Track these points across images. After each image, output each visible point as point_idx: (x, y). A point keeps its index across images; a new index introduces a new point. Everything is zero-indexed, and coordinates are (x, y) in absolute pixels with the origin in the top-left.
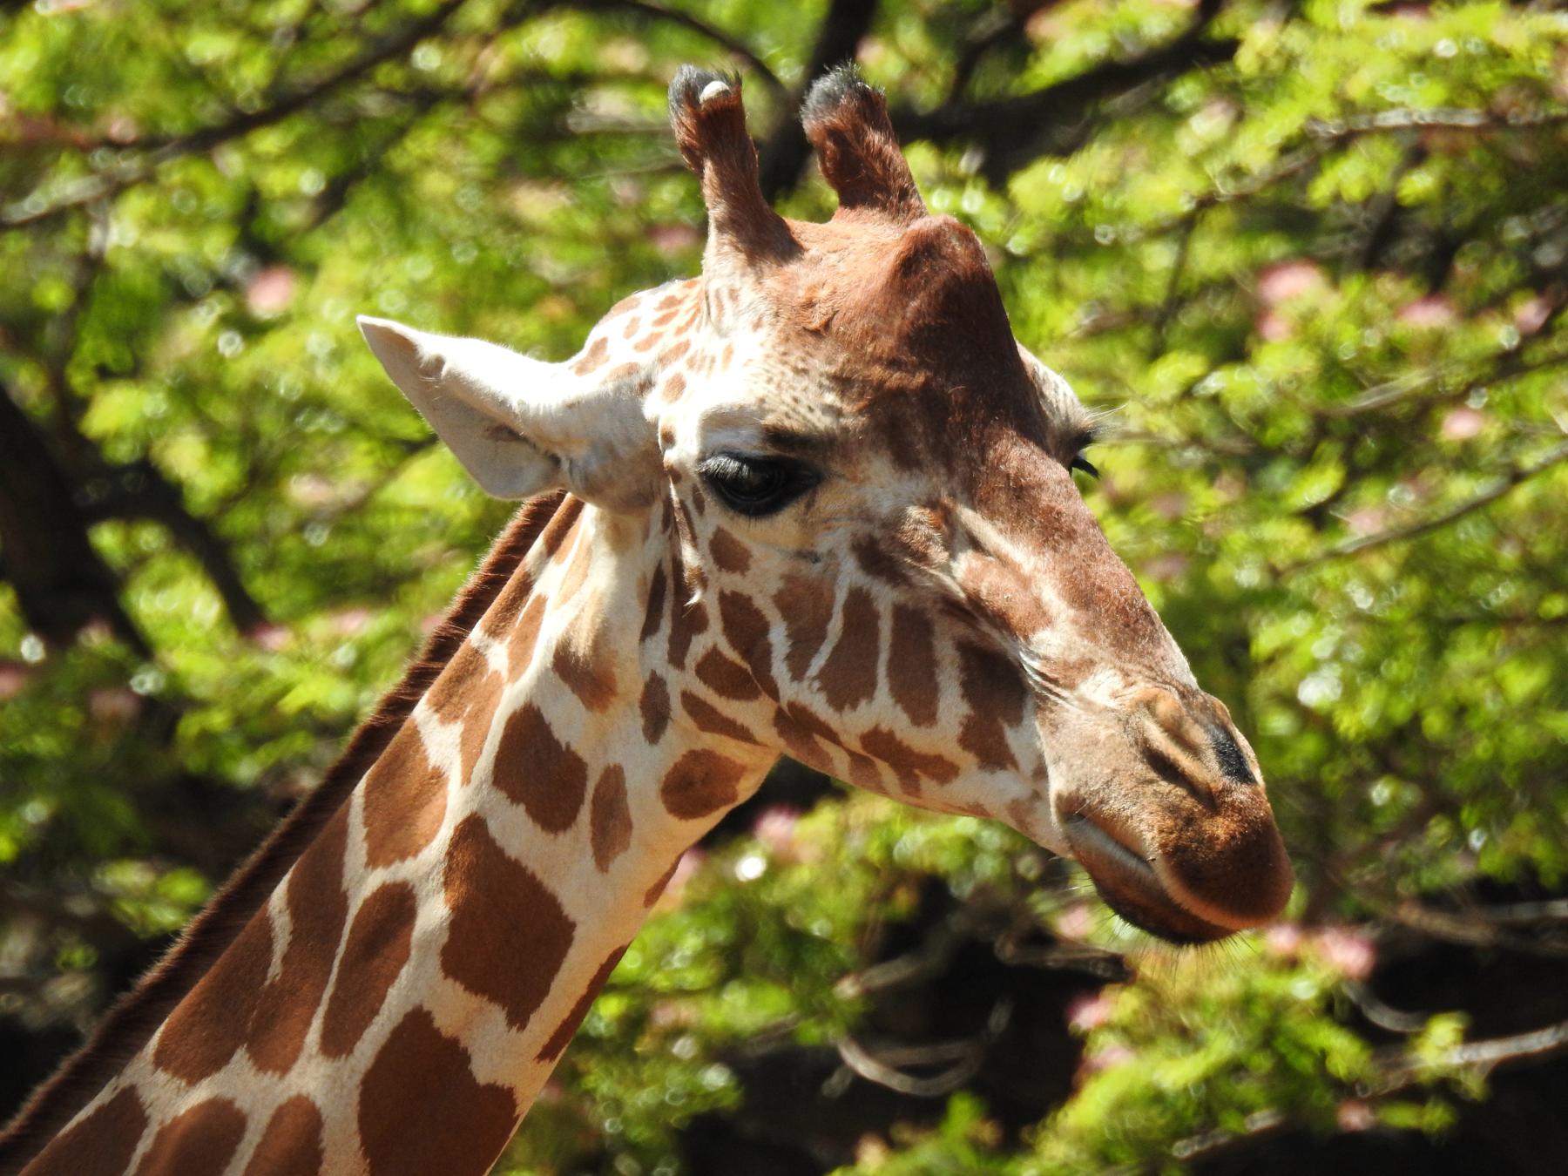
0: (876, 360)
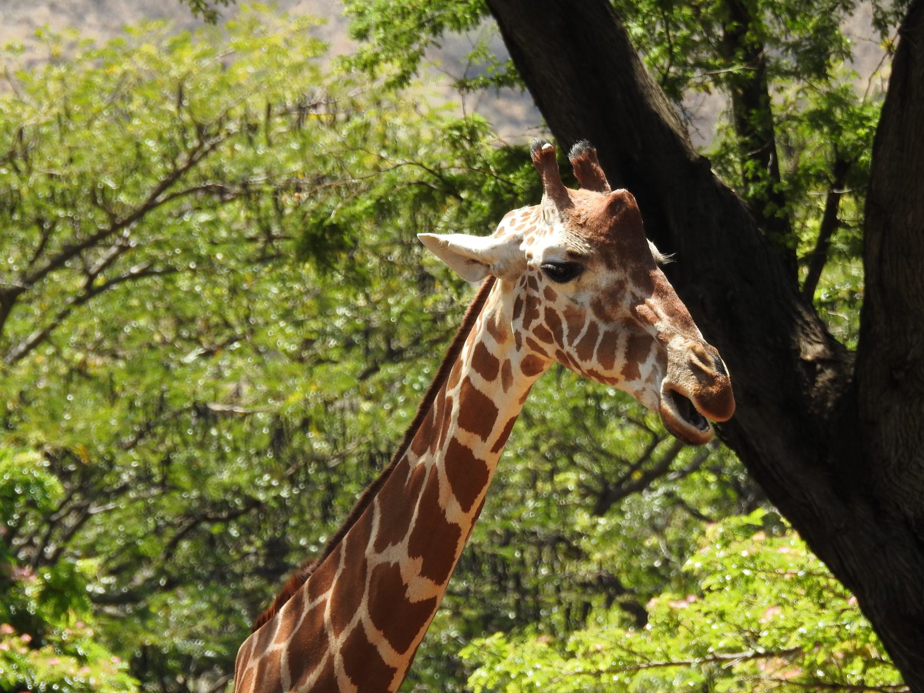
0: (601, 234)
